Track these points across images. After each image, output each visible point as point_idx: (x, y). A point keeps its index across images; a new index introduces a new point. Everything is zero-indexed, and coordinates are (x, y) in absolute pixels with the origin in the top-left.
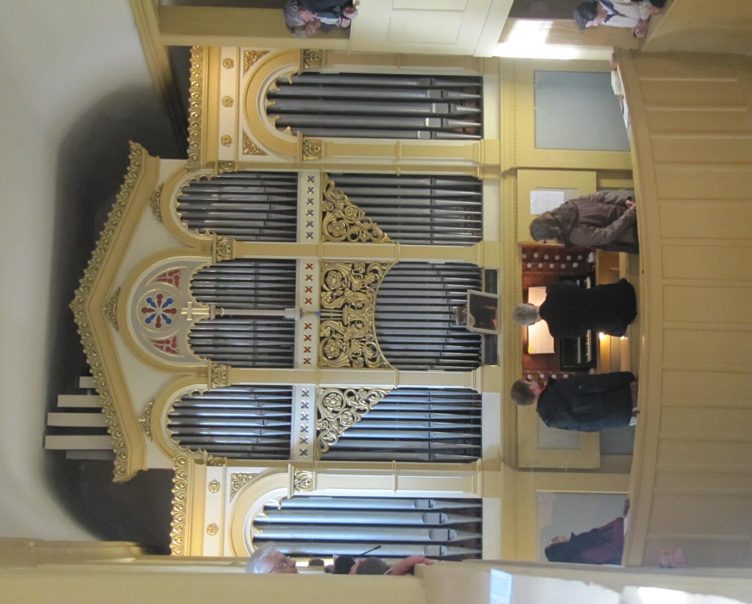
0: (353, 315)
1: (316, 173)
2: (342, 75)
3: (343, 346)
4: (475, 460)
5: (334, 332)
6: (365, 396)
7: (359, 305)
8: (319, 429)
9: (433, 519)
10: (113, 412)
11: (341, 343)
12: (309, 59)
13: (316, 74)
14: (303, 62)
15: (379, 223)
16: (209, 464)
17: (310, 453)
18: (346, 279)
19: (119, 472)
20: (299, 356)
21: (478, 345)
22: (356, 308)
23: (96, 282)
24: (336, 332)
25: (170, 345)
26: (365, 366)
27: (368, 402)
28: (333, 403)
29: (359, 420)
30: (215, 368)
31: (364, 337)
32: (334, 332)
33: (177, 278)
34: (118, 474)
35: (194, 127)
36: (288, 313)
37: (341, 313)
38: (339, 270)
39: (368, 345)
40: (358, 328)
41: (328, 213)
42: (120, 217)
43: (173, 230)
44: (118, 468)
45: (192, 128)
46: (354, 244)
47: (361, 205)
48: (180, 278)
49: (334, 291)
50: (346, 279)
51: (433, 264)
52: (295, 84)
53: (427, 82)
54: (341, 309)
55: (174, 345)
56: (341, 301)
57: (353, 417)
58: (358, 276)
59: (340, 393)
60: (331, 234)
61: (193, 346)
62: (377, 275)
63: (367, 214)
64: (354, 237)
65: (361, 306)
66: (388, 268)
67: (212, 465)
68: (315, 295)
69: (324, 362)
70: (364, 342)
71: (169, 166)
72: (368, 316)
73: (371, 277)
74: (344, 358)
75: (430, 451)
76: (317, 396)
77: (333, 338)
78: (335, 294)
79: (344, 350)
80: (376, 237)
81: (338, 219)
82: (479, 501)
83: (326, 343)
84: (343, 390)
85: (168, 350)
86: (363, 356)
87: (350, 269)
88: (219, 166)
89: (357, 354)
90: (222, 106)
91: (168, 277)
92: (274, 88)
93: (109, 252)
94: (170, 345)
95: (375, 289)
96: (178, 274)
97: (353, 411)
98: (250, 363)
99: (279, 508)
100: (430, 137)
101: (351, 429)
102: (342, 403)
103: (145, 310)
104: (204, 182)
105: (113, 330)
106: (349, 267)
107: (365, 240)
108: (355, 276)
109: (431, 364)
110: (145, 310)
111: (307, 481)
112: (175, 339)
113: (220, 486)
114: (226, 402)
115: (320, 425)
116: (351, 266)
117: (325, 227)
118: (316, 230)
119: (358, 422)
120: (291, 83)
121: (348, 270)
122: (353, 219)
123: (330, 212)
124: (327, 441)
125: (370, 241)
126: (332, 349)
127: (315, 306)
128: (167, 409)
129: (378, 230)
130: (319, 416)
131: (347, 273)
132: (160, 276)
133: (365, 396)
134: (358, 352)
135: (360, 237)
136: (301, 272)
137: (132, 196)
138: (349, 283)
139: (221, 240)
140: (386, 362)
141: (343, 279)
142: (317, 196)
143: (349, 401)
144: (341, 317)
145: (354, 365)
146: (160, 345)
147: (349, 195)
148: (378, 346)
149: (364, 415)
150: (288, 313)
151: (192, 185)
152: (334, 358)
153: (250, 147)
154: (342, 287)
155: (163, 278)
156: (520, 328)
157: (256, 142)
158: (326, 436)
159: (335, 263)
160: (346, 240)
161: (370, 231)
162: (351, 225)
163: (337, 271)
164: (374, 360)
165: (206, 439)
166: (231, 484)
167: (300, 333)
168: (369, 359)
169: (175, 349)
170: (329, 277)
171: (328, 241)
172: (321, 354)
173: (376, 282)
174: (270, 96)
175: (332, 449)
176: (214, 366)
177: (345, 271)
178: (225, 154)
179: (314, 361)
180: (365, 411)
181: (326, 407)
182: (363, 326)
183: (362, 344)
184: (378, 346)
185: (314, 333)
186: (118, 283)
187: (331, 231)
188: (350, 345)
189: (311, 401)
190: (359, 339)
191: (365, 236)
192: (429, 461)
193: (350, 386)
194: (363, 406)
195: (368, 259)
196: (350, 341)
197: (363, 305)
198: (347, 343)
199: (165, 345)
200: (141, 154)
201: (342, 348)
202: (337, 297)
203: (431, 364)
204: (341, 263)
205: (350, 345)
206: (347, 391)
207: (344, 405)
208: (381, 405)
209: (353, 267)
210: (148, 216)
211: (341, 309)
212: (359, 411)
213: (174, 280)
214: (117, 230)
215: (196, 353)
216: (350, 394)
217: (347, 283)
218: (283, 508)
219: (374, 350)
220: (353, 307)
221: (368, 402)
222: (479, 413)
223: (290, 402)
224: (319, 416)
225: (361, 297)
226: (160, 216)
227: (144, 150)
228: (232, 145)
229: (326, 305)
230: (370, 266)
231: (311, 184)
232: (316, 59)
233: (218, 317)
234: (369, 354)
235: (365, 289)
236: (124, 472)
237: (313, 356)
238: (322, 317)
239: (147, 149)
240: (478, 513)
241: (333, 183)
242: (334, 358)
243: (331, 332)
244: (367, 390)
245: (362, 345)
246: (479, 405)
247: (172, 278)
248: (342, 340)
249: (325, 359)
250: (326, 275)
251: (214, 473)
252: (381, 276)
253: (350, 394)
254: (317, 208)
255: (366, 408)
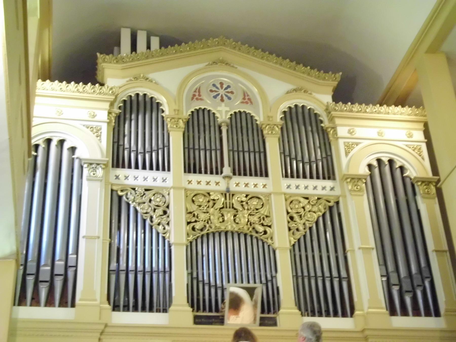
0: (229, 216)
1: (337, 192)
2: (418, 212)
3: (203, 207)
4: (109, 303)
5: (214, 202)
6: (164, 222)
7: (237, 220)
8: (136, 189)
9: (59, 264)
10: (147, 57)
11: (206, 206)
12: (426, 185)
13: (415, 194)
14: (423, 180)
15: (305, 236)
16: (110, 113)
17: (117, 182)
18: (257, 211)
19: (104, 57)
20: (194, 177)
21: (210, 310)
22: (235, 218)
23: (239, 53)
24: (214, 204)
25: (197, 97)
26: (189, 223)
27: (159, 224)
28: (158, 200)
29: (145, 218)
30: (182, 120)
31: (211, 223)
32: (214, 202)
33: (247, 103)
34: (103, 57)
35: (359, 107)
36: (227, 170)
37: (230, 208)
38: (264, 207)
39: (205, 226)
40: (218, 219)
41: (308, 201)
42: (286, 67)
43: (280, 101)
44: (107, 57)
45: (358, 106)
46: (286, 218)
47: (317, 223)
48: (247, 105)
49: (247, 203)
50: (257, 211)
51: (275, 277)
52: (403, 179)
53: (426, 274)
54: (233, 207)
55: (197, 99)
56: (240, 208)
57: (146, 213)
58: (260, 220)
59: (166, 205)
60: (291, 202)
61: (198, 111)
62: (263, 233)
63: (310, 229)
64: (292, 218)
65: (237, 222)
66: (270, 241)
67: (108, 115)
68: (242, 188)
69: (190, 194)
70: (208, 223)
71: (327, 98)
72: (230, 226)
73: (261, 229)
74: (193, 208)
75: (118, 272)
76: (163, 188)
77: (209, 202)
78: (244, 203)
79: (201, 208)
80: (293, 234)
81: (303, 208)
82: (73, 305)
83: (205, 196)
84: (168, 207)
85: (194, 95)
86: (196, 221)
87: (266, 214)
88: (333, 128)
89: (197, 217)
90: (378, 130)
91: (247, 98)
92: (398, 165)
93: (261, 60)
94: (197, 97)
95: (251, 232)
96: (249, 103)
97: (152, 213)
98: (186, 146)
99: (73, 157)
100: (382, 275)
101: (136, 212)
102: (158, 206)
103: (222, 84)
104: (319, 122)
105: (207, 63)
106: (267, 213)
107: (290, 226)
108: (260, 218)
109: (192, 274)
110: (222, 84)
111: (95, 173)
112: (201, 99)
113: (92, 118)
114: (157, 237)
115: (140, 191)
116: (268, 215)
117: (296, 198)
118: (293, 190)
119: (142, 216)
120: (404, 175)
121: (265, 212)
122: (306, 218)
123: (309, 202)
124: (127, 194)
125: (290, 229)
126: (201, 199)
127: (233, 188)
128: (151, 93)
129: (298, 235)
130: (146, 190)
131: (262, 212)
132: (247, 93)
133: (164, 222)
134: (199, 218)
135: (291, 222)
136: (260, 181)
137: (302, 75)
138: (254, 213)
139: (278, 127)
140: (191, 238)
141: (257, 209)
142: (319, 192)
143: (159, 211)
144: (226, 207)
145: (188, 215)
146: (197, 91)
147: (324, 215)
148: (205, 232)
149: (148, 222)
150: (227, 170)
151: (316, 114)
152: (193, 201)
153: (349, 148)
154: (251, 209)
155: (246, 95)
156: (242, 112)
157: (357, 148)
158: (131, 194)
159: (269, 203)
160: (288, 213)
161: (298, 230)
162: (301, 216)
163: (263, 205)
164: (193, 229)
165: (128, 116)
166: (94, 125)
167: (213, 178)
168: (194, 226)
169: (195, 99)
170: (257, 200)
171: (286, 200)
172: (196, 192)
173: (257, 232)
174: (391, 162)
175: (120, 198)
176: (183, 119)
177: (265, 211)
178: (342, 131)
179: (190, 186)
180: (152, 221)
181: (154, 195)
182: (220, 222)
183: (206, 221)
184: (205, 232)
185: (213, 187)
186: (240, 68)
187: (293, 202)
188: (205, 213)
189: (159, 183)
190: (210, 219)
191: (292, 225)
192: (109, 271)
193: (171, 212)
194: (156, 221)
195: (275, 226)
196: (207, 212)
197: (237, 223)
198: (206, 210)
199: (197, 94)
200: (333, 81)
201: (202, 207)
202: (242, 205)
203: (192, 274)
204: (269, 208)
205: (205, 213)
206: (167, 210)
207: (156, 207)
208: (157, 234)
209: (267, 216)
210: (291, 87)
211: (233, 207)
212: (151, 217)
213: (245, 101)
214: (278, 66)
215: (192, 112)
216: (165, 213)
217: (254, 212)
218: (73, 159)
219: (202, 230)
220: (235, 216)
221: (159, 224)
222: (151, 310)
223: (158, 169)
224: (146, 190)
225: (244, 221)
226: (291, 92)
227: (336, 83)
228: (349, 135)
229: (236, 198)
230: (269, 228)
231: (328, 188)
232: (427, 190)
233: (220, 127)
234: (198, 226)
235: (251, 225)
236: (104, 61)
237: (194, 186)
238: (226, 195)
239: (338, 85)
240: (63, 303)
241: (331, 204)
242: (193, 201)
243: (214, 200)
244: (168, 224)
245: (205, 221)
246: (158, 311)
247: (247, 100)
248: (208, 207)
249: (193, 195)
250: (259, 198)
251: (103, 115)
252: (263, 237)
253: (165, 213)
254: (310, 191)
255: (154, 223)
